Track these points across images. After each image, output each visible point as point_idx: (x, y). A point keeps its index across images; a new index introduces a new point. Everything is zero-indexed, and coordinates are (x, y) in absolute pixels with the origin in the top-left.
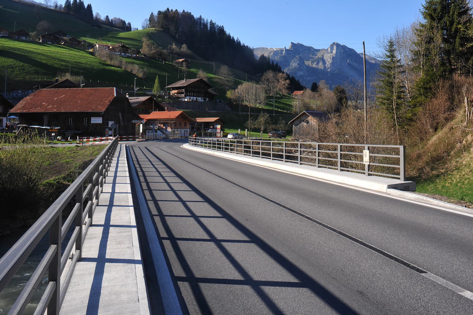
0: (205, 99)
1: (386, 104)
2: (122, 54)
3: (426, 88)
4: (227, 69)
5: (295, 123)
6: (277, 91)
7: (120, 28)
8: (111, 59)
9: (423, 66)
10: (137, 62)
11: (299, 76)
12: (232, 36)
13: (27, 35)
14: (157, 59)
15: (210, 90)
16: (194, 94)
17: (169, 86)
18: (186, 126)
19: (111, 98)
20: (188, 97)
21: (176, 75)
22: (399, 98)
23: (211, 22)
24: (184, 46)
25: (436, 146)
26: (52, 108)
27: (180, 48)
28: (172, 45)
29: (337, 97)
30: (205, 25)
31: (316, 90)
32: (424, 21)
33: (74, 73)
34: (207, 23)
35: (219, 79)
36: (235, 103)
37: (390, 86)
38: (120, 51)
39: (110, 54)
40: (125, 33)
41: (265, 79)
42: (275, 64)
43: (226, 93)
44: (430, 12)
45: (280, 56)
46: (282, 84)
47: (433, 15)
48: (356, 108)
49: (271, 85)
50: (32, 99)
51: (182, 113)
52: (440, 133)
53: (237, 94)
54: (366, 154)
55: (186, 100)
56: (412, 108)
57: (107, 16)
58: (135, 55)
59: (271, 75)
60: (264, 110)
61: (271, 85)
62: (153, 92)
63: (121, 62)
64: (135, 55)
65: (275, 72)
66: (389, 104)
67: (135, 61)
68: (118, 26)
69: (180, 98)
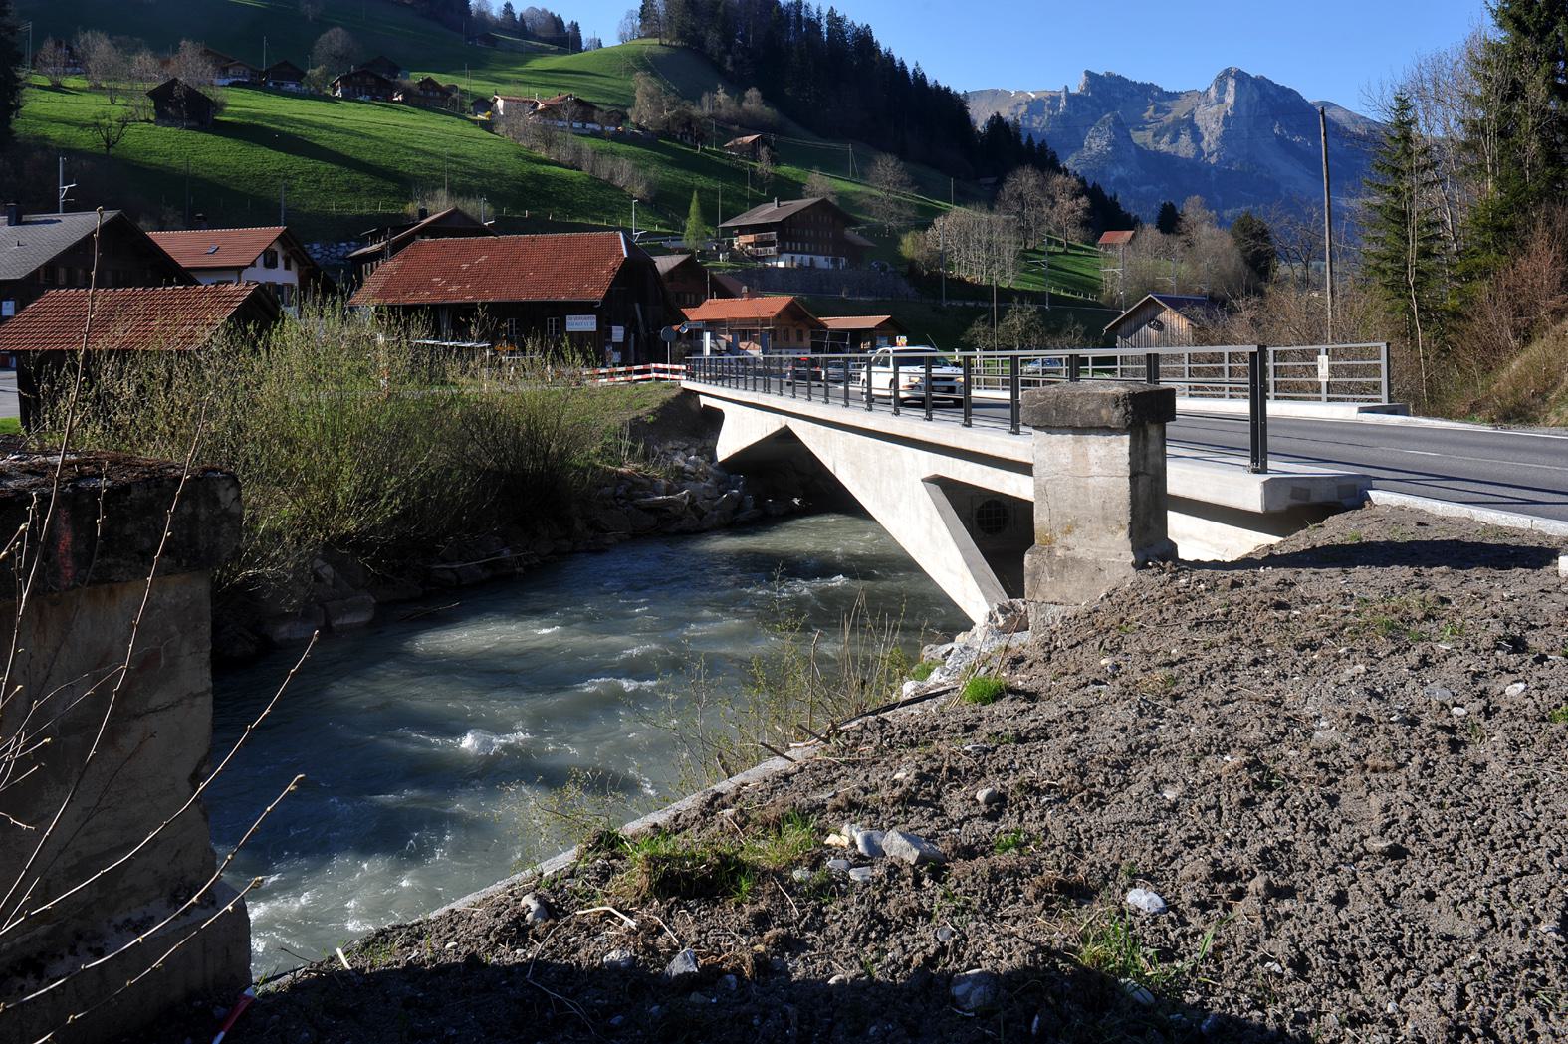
0: (835, 262)
1: (1389, 272)
2: (576, 125)
3: (1499, 229)
4: (894, 167)
5: (1124, 328)
6: (1049, 232)
7: (551, 41)
8: (549, 143)
9: (1494, 169)
10: (624, 148)
11: (1115, 180)
12: (897, 57)
13: (298, 75)
14: (678, 137)
15: (850, 233)
16: (803, 246)
17: (729, 224)
18: (801, 339)
19: (614, 263)
20: (788, 256)
21: (748, 188)
22: (1425, 253)
23: (832, 13)
24: (752, 93)
25: (1518, 383)
26: (459, 290)
27: (742, 98)
28: (715, 91)
29: (1244, 251)
30: (814, 25)
31: (1175, 228)
32: (1499, 36)
33: (460, 191)
34: (819, 19)
35: (871, 196)
36: (926, 272)
37: (1399, 223)
38: (574, 118)
39: (545, 127)
40: (568, 57)
41: (1012, 197)
42: (1036, 145)
43: (898, 241)
44: (1515, 9)
45: (1049, 116)
46: (1069, 207)
47: (1525, 17)
48: (1305, 283)
49: (1031, 214)
50: (400, 268)
51: (792, 303)
52: (1536, 350)
53: (930, 244)
54: (1323, 362)
55: (781, 264)
56: (1463, 282)
57: (508, 6)
58: (613, 129)
59: (1032, 181)
60: (1024, 295)
61: (1031, 214)
62: (684, 241)
63: (578, 151)
64: (613, 129)
65: (1043, 171)
66: (1397, 272)
67: (616, 146)
68: (543, 35)
69: (763, 259)
